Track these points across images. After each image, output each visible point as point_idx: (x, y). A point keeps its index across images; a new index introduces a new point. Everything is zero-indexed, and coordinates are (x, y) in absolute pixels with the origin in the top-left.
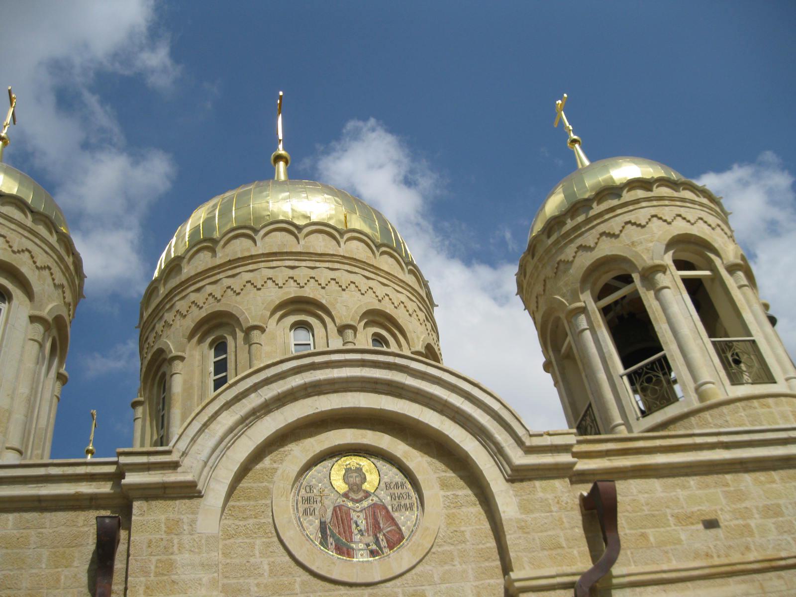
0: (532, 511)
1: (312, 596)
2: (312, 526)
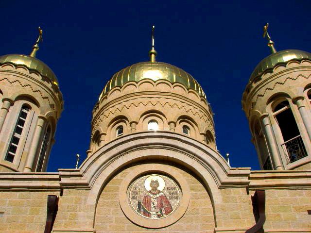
0: (228, 202)
1: (131, 232)
2: (134, 204)
